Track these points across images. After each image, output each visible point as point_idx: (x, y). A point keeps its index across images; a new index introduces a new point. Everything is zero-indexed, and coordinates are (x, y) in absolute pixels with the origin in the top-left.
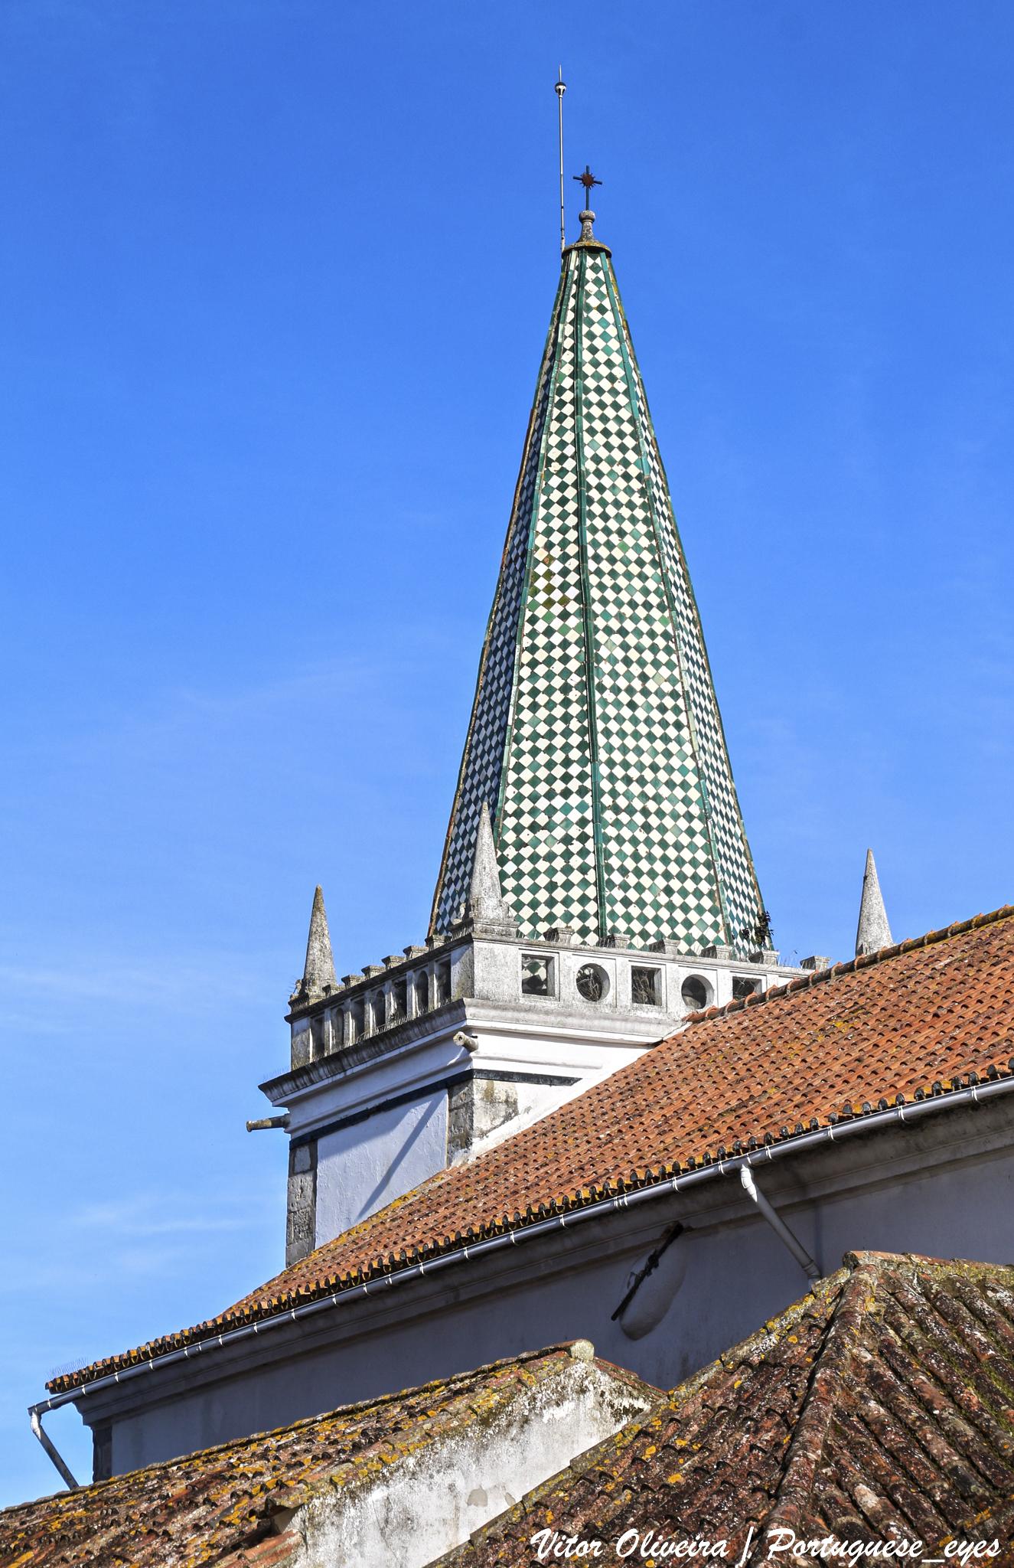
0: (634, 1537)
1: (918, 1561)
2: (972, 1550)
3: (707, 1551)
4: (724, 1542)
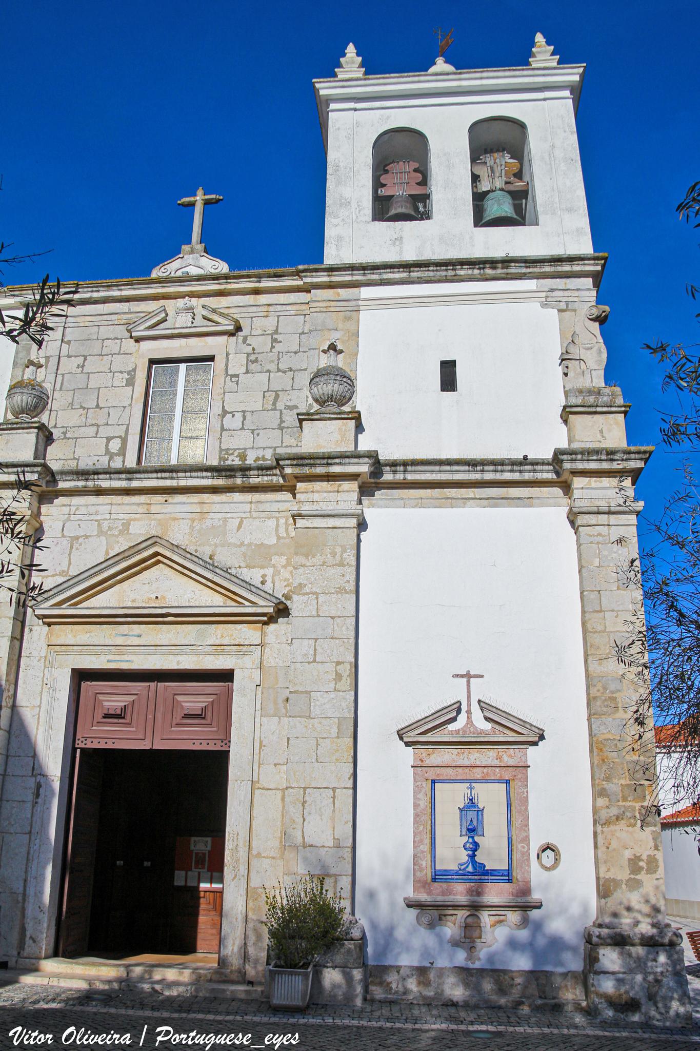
0: (73, 1032)
1: (248, 1046)
2: (282, 1039)
3: (185, 1040)
4: (128, 1035)
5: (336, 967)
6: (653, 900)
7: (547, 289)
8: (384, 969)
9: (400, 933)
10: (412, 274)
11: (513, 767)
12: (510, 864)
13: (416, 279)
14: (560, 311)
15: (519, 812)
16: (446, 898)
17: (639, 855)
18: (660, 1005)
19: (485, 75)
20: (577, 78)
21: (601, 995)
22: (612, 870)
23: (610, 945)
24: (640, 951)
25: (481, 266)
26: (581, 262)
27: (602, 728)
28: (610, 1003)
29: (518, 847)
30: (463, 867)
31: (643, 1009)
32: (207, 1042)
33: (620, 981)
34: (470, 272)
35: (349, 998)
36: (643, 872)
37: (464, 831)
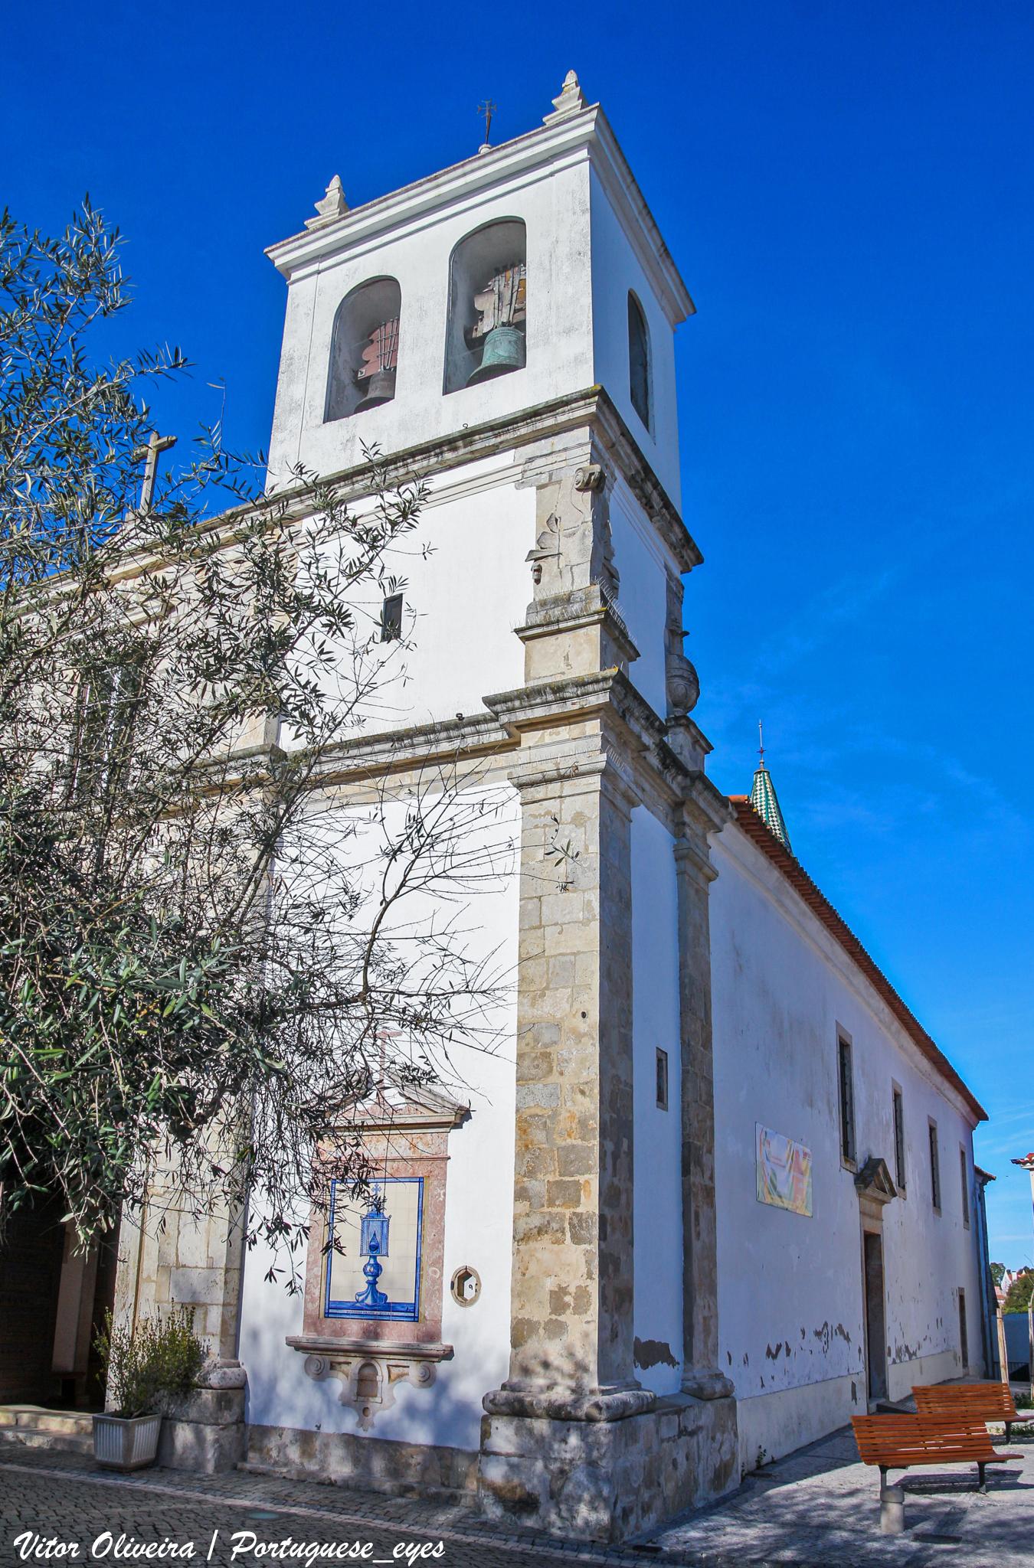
5: (191, 1422)
6: (580, 1354)
7: (523, 461)
8: (265, 1431)
9: (284, 1387)
10: (356, 485)
11: (428, 1159)
12: (417, 1296)
13: (362, 491)
14: (540, 488)
15: (433, 1223)
16: (335, 1340)
17: (564, 1285)
18: (563, 1507)
19: (468, 168)
20: (591, 127)
21: (489, 1485)
22: (527, 1306)
23: (507, 1415)
24: (542, 1426)
25: (438, 451)
26: (566, 408)
27: (529, 1099)
28: (500, 1498)
29: (428, 1271)
30: (361, 1298)
31: (541, 1511)
32: (308, 1555)
33: (513, 1467)
34: (425, 463)
35: (199, 1465)
36: (569, 1311)
37: (366, 1248)
